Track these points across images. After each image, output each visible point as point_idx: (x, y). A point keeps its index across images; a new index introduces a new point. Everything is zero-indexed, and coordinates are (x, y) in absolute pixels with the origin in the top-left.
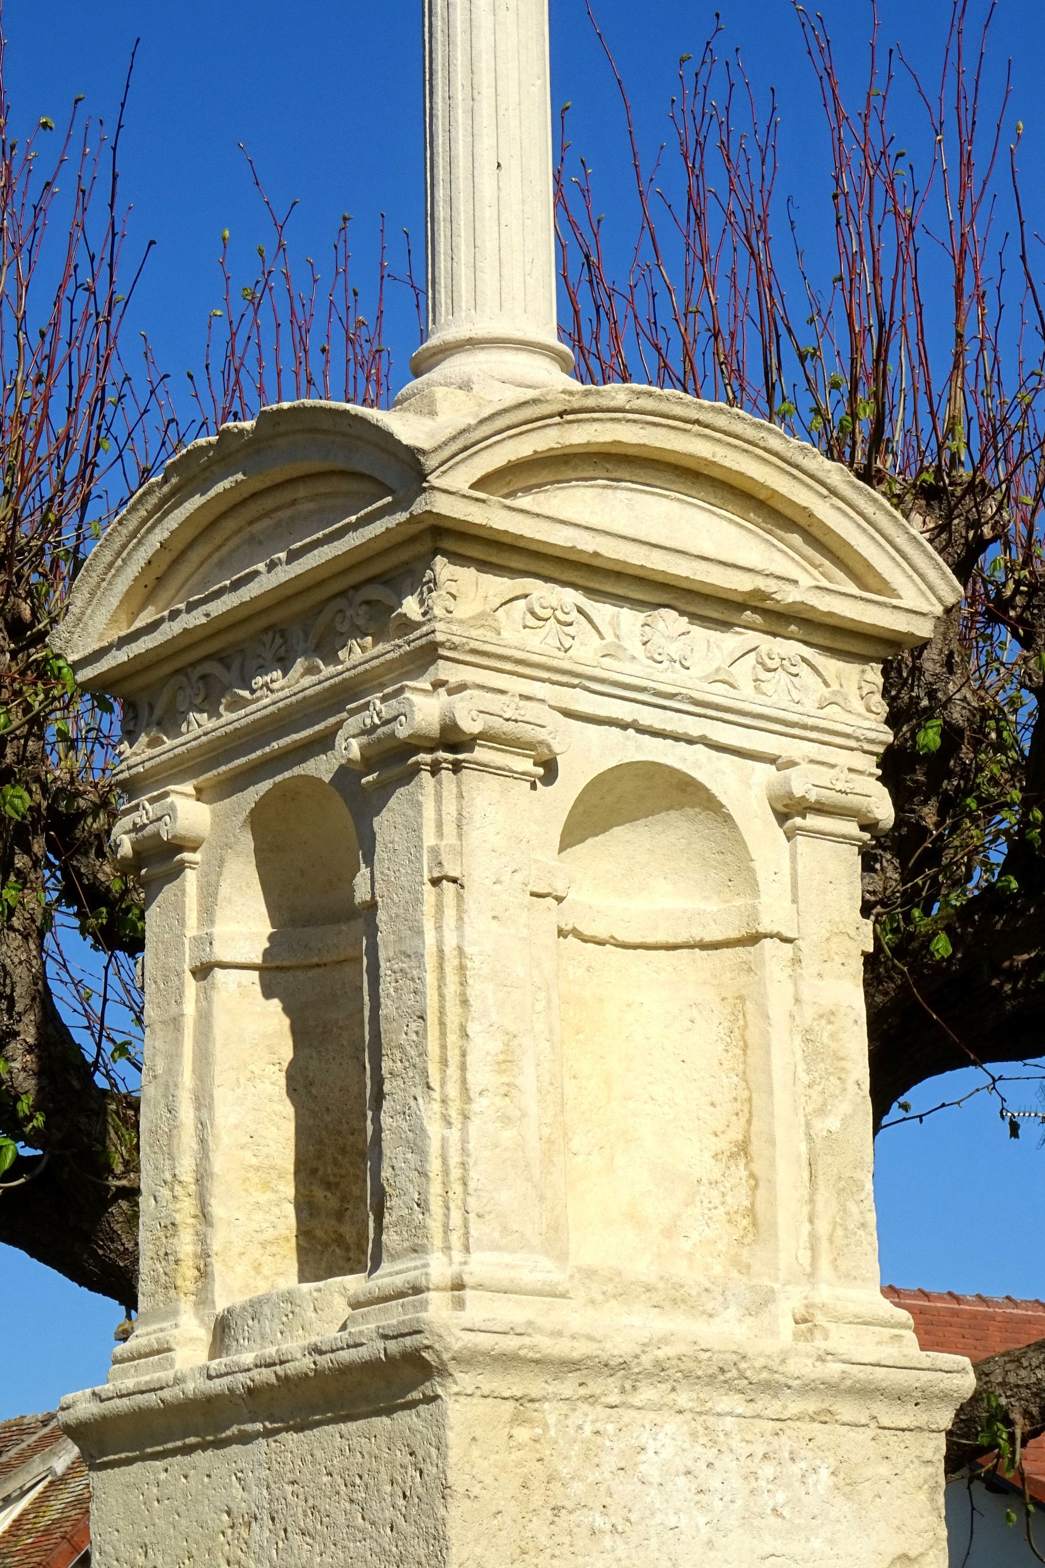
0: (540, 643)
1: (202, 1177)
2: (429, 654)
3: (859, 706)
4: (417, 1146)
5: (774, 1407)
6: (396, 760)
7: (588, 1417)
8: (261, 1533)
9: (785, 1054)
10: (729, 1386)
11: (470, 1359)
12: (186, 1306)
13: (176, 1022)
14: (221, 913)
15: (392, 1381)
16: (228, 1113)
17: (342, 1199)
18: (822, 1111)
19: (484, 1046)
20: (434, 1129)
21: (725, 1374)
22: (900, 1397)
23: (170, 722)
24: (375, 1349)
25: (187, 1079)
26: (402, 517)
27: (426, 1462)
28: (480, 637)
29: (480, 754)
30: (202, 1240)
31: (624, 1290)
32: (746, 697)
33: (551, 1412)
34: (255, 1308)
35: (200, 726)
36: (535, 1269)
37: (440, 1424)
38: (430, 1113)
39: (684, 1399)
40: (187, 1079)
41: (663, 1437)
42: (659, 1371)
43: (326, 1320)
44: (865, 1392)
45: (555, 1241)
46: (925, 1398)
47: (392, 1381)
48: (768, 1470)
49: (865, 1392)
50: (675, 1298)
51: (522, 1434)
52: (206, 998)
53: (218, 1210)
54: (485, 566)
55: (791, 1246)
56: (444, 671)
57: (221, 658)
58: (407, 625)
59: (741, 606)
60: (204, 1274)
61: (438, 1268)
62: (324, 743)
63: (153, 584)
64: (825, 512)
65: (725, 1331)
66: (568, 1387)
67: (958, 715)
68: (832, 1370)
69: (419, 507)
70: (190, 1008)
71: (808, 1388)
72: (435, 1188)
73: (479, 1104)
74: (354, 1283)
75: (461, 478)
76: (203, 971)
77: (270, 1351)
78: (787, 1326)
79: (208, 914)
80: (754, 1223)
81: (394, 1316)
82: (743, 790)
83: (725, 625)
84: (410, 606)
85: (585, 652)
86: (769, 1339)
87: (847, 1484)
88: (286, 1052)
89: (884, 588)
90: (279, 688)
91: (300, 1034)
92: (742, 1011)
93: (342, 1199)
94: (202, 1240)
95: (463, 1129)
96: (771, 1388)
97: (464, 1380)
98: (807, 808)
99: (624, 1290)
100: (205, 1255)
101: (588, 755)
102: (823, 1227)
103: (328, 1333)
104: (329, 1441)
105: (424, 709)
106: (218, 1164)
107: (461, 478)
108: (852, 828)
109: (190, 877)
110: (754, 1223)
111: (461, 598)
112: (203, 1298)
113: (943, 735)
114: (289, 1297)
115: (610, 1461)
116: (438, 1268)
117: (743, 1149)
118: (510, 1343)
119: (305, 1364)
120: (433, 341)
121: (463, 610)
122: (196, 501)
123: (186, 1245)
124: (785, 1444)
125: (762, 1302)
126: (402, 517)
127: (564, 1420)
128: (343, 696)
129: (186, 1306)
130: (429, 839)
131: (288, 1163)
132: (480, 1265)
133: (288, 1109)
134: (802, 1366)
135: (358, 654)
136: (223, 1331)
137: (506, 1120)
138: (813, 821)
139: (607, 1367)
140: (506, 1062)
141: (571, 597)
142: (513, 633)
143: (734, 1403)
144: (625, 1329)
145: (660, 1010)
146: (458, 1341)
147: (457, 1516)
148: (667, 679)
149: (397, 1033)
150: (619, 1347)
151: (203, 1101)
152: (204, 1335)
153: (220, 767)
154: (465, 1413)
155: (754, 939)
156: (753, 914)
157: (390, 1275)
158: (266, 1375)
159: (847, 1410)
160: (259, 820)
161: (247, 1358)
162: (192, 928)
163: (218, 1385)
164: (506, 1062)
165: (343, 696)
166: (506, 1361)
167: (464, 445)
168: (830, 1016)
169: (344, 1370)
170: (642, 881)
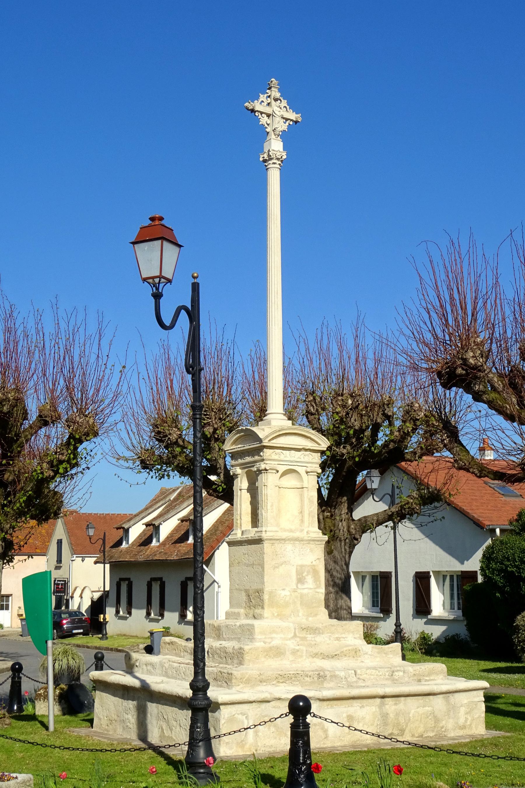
0: (276, 457)
1: (241, 514)
2: (263, 460)
3: (317, 458)
4: (262, 515)
5: (303, 543)
6: (260, 471)
7: (280, 545)
8: (246, 556)
9: (306, 501)
10: (297, 541)
11: (267, 539)
12: (239, 529)
13: (237, 496)
14: (243, 483)
15: (259, 541)
16: (243, 506)
17: (255, 520)
18: (310, 508)
19: (269, 505)
20: (264, 514)
21: (297, 539)
22: (318, 541)
23: (236, 459)
24: (257, 538)
25: (239, 502)
26: (260, 445)
27: (262, 549)
28: (270, 458)
29: (269, 471)
30: (241, 521)
31: (285, 530)
32: (302, 460)
33: (276, 545)
34: (246, 531)
35: (240, 461)
36: (275, 529)
37: (263, 546)
38: (263, 512)
39: (292, 542)
40: (239, 502)
41: (289, 547)
42: (289, 539)
43: (252, 533)
44: (314, 540)
45: (278, 525)
46: (321, 541)
47: (259, 541)
48: (302, 550)
49: (314, 540)
50: (291, 531)
51: (273, 547)
52: (241, 492)
53: (242, 518)
54: (270, 449)
55: (306, 523)
56: (265, 462)
57: (242, 453)
58: (261, 456)
59: (301, 449)
60: (241, 525)
61: (264, 529)
62: (253, 466)
63: (234, 443)
64: (312, 437)
65: (297, 534)
66: (278, 542)
67: (357, 428)
68: (310, 538)
69: (262, 444)
70: (239, 494)
71: (307, 540)
72: (264, 520)
73: (269, 511)
74: (256, 529)
75: (267, 441)
76: (240, 490)
77: (247, 536)
78: (305, 533)
79: (241, 483)
80: (302, 521)
81: (259, 534)
82: (302, 471)
83: (300, 451)
84: (261, 454)
85: (282, 457)
86: (303, 535)
87: (311, 550)
88: (250, 499)
89: (319, 445)
90: (248, 459)
91: (251, 497)
92: (301, 496)
93: (255, 520)
94: (241, 521)
95: (267, 513)
96: (302, 541)
97: (266, 542)
98: (309, 472)
99: (285, 530)
100: (241, 523)
101: (282, 469)
102: (310, 521)
103: (253, 535)
104: (253, 546)
105: (263, 466)
106: (242, 513)
107: (267, 441)
108: (316, 474)
109: (239, 478)
110: (302, 521)
111: (267, 453)
112: (241, 528)
113: (354, 432)
114: (249, 530)
115: (283, 549)
116: (264, 529)
117: (301, 512)
118: (271, 538)
119: (250, 538)
120: (267, 412)
121: (267, 455)
122: (238, 435)
123: (239, 522)
124: (304, 547)
125: (302, 531)
126: (260, 445)
127: (278, 546)
128: (255, 462)
129: (239, 529)
130: (263, 481)
131: (250, 512)
132: (268, 529)
133: (250, 506)
134: (306, 538)
135: (257, 458)
136: (243, 533)
137: (272, 512)
138: (311, 473)
139: (282, 539)
140: (272, 506)
141: (281, 451)
142: (274, 457)
143: (298, 542)
144: (284, 535)
145: (292, 497)
146: (265, 538)
147: (265, 556)
148: (292, 459)
149: (260, 502)
150: (284, 537)
151: (241, 505)
152: (241, 532)
153: (243, 466)
154: (266, 545)
155: (303, 488)
156: (303, 485)
157: (259, 529)
158: (246, 539)
159: (311, 543)
160: (246, 473)
161: (245, 537)
162: (239, 485)
163: (242, 539)
164: (272, 506)
165: (255, 462)
166: (271, 539)
167: (267, 437)
168: (312, 496)
169: (254, 539)
170: (290, 481)
